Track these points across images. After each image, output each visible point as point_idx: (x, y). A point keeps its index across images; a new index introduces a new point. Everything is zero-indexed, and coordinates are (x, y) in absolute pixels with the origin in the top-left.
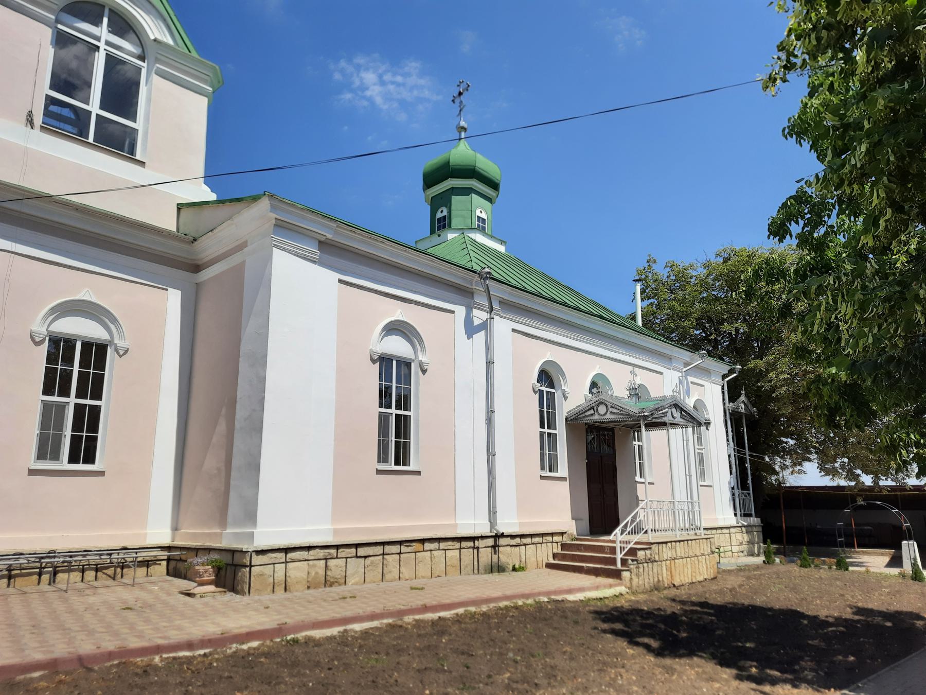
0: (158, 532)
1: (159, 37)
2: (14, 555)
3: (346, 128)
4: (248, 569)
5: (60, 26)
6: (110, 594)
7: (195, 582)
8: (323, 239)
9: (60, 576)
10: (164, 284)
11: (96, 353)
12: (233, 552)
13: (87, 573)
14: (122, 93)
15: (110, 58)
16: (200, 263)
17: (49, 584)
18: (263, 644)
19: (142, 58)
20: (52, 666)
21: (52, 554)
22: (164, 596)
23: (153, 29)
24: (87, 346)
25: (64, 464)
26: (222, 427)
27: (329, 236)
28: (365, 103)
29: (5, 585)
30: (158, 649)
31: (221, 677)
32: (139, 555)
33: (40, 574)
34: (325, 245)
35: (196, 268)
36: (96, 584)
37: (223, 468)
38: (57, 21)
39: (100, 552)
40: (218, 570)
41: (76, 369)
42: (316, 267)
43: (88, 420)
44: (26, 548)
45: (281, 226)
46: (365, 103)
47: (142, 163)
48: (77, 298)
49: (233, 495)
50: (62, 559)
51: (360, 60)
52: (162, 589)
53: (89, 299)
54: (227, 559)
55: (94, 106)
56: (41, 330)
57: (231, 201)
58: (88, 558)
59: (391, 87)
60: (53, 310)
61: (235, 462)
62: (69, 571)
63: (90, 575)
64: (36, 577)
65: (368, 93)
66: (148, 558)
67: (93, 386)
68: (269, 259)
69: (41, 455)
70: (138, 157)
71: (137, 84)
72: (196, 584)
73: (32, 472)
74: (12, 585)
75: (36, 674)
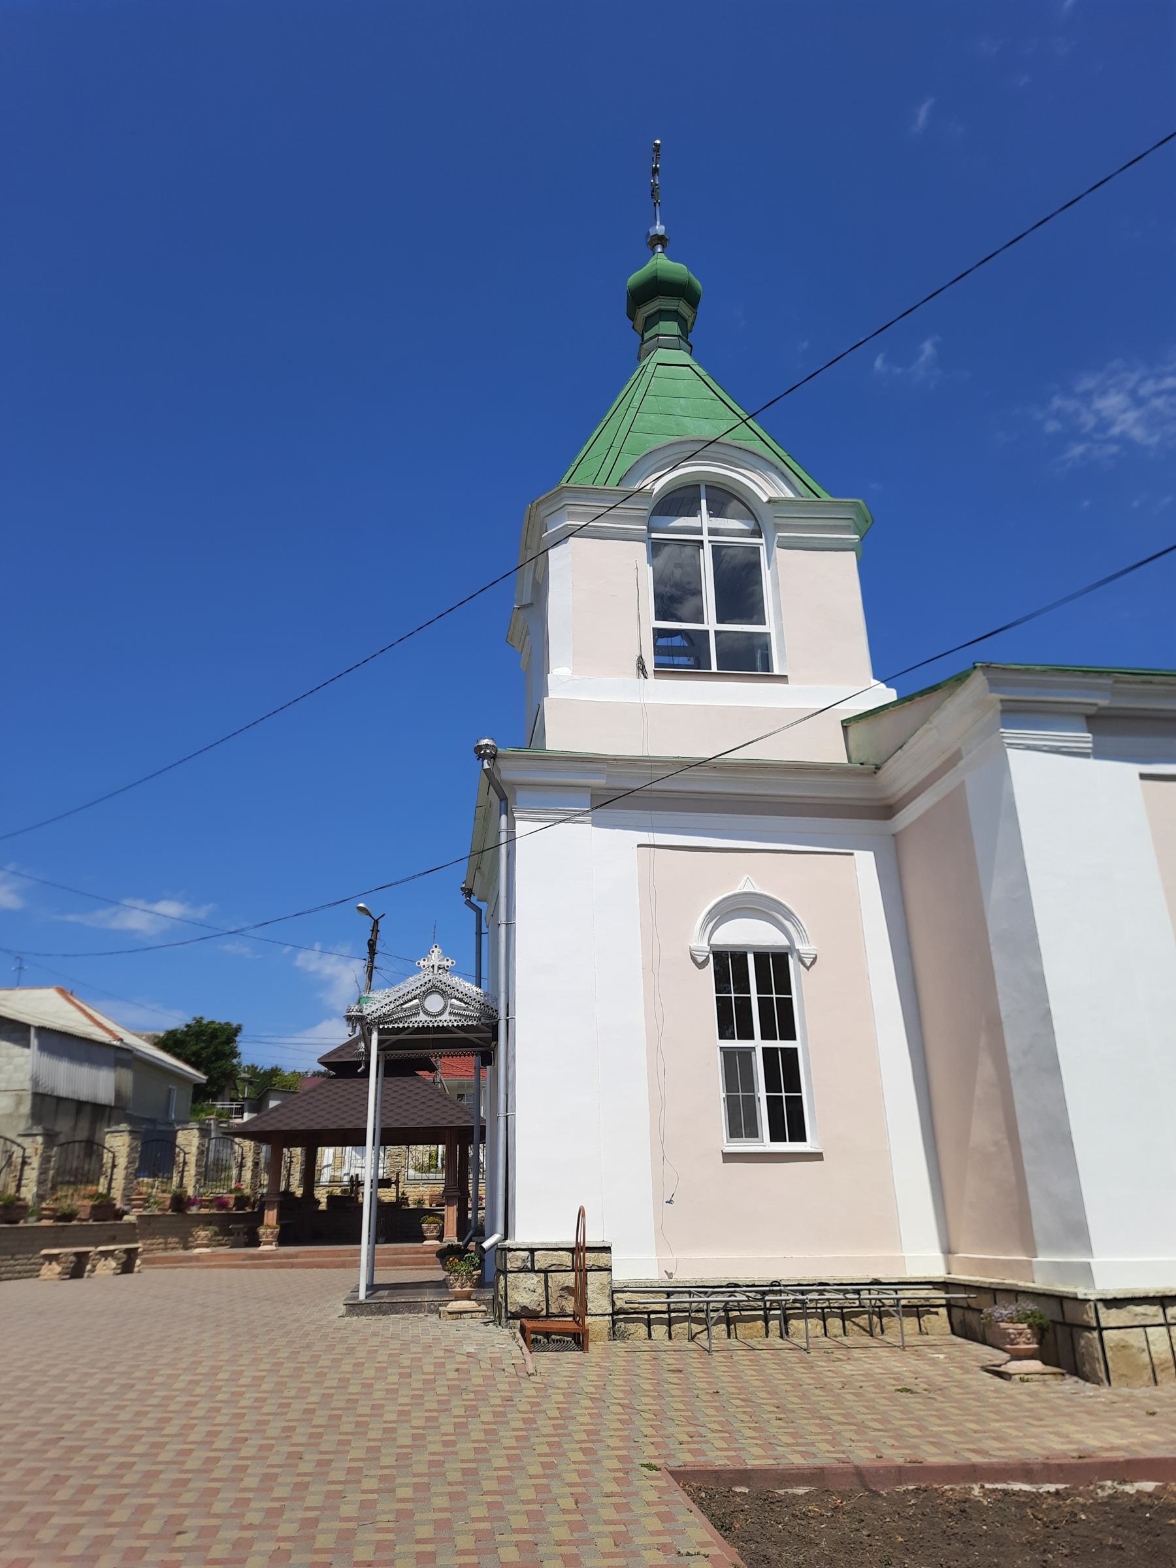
0: (920, 1258)
1: (773, 494)
2: (728, 1286)
3: (1086, 503)
4: (1096, 1334)
5: (654, 535)
6: (875, 1362)
7: (1005, 1351)
8: (1092, 711)
9: (793, 1323)
10: (846, 845)
11: (775, 966)
12: (1061, 1299)
13: (829, 1320)
14: (740, 590)
15: (717, 550)
16: (892, 801)
17: (781, 1337)
18: (1164, 1488)
19: (757, 533)
20: (816, 1476)
21: (775, 1286)
22: (958, 1374)
23: (765, 487)
24: (761, 958)
25: (765, 1144)
26: (986, 1069)
27: (1103, 702)
28: (1113, 449)
29: (725, 1334)
30: (974, 1473)
31: (1101, 1546)
32: (900, 1295)
33: (766, 1320)
34: (1096, 721)
35: (888, 811)
36: (846, 1341)
37: (1006, 1142)
38: (650, 530)
39: (843, 1287)
40: (1041, 1332)
41: (754, 992)
42: (1091, 762)
43: (784, 1070)
44: (742, 1275)
45: (1017, 713)
46: (1113, 449)
47: (783, 678)
48: (737, 891)
49: (1032, 1189)
50: (791, 1297)
51: (1088, 383)
52: (949, 1356)
53: (753, 890)
54: (1050, 1312)
55: (711, 624)
56: (702, 946)
57: (922, 693)
58: (828, 1295)
59: (1159, 403)
60: (711, 914)
61: (1025, 1131)
62: (805, 1316)
63: (835, 1324)
64: (760, 1323)
65: (1116, 430)
66: (915, 1302)
67: (781, 1020)
68: (1003, 767)
69: (735, 1132)
70: (776, 672)
71: (757, 565)
72: (1006, 1356)
73: (729, 1157)
74: (733, 1335)
75: (801, 1491)
